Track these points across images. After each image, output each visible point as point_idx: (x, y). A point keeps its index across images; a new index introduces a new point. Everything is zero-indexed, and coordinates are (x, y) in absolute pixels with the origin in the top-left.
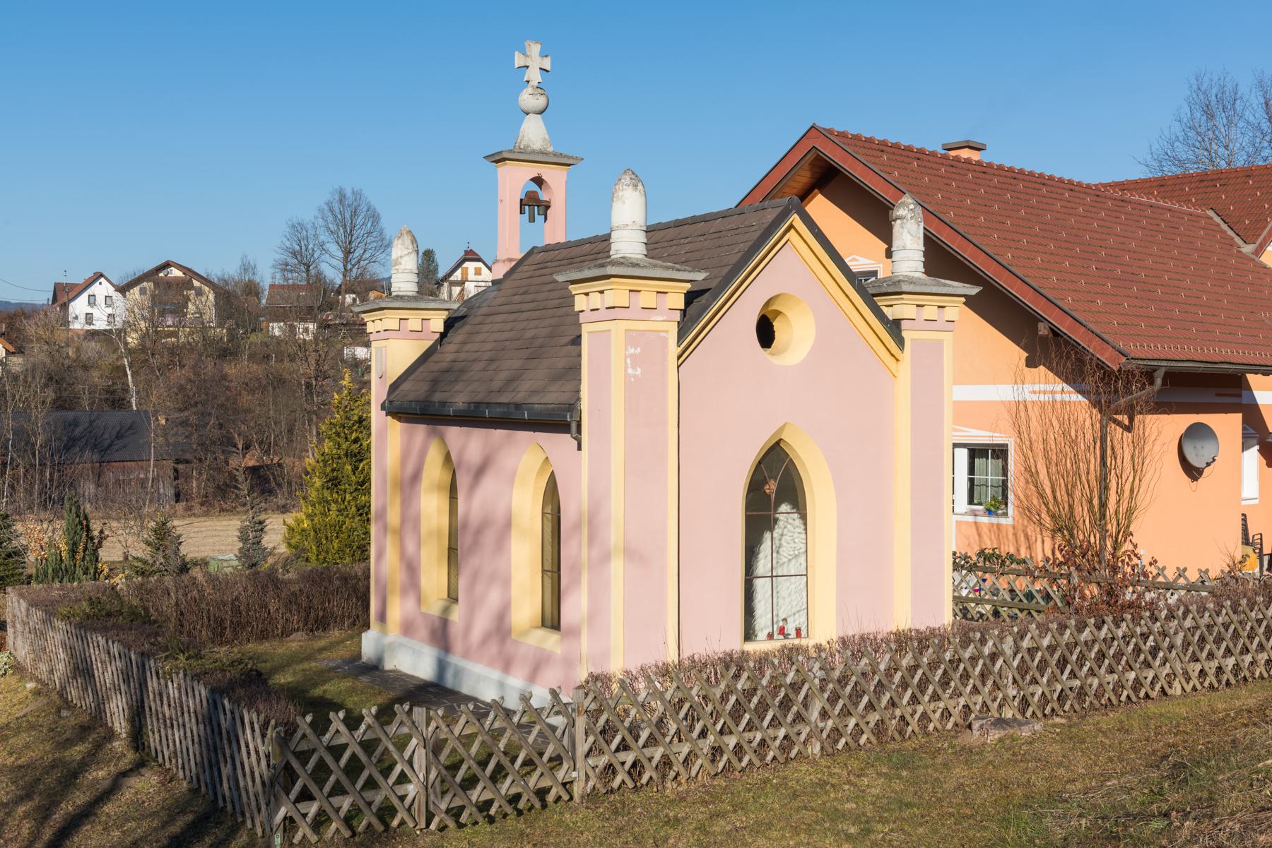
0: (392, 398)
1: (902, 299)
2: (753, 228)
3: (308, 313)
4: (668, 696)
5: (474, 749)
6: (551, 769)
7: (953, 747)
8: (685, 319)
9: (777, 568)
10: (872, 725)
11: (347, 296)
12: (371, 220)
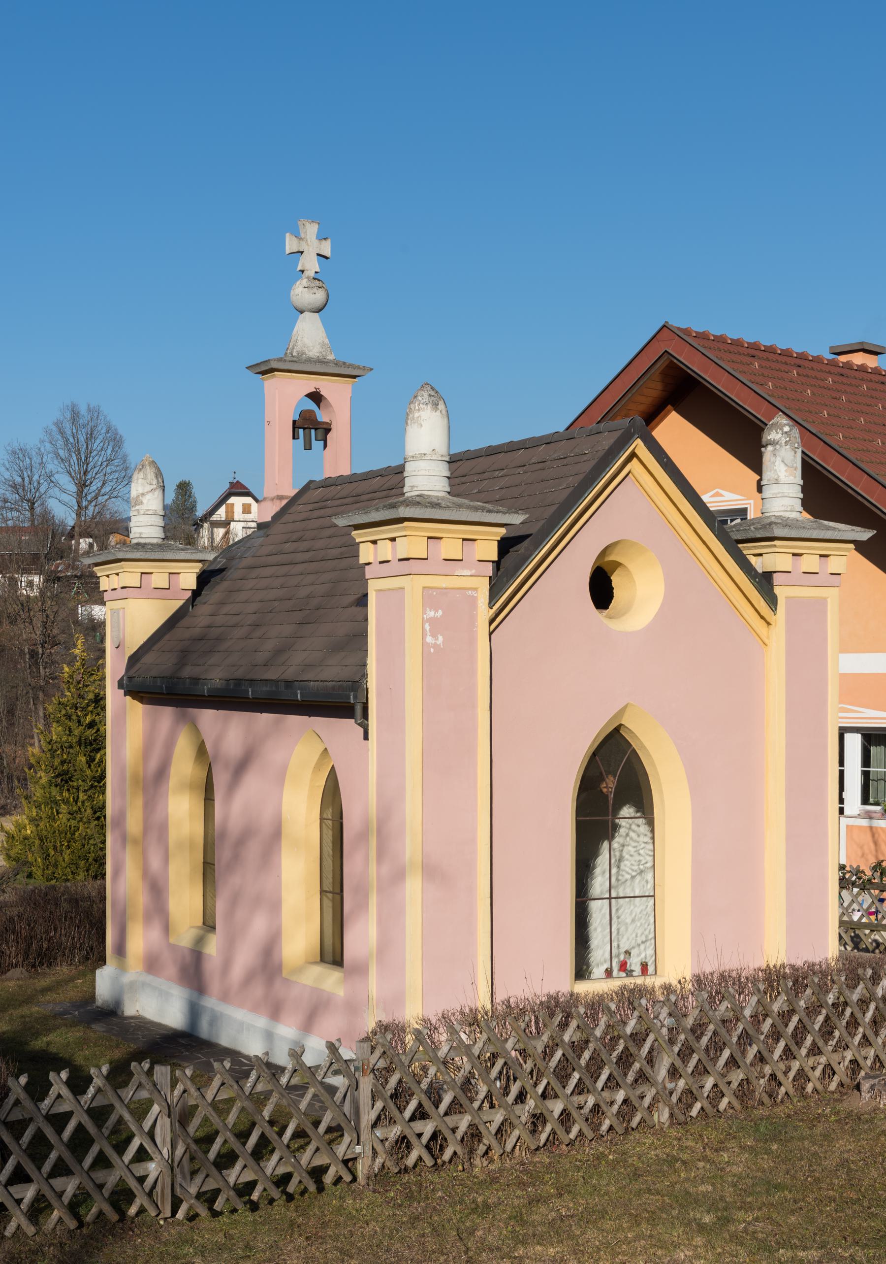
0: (131, 673)
1: (775, 546)
2: (585, 458)
3: (32, 563)
4: (476, 1051)
5: (231, 1118)
6: (330, 1143)
7: (837, 1113)
8: (499, 573)
9: (617, 887)
10: (735, 1085)
11: (81, 540)
12: (111, 444)
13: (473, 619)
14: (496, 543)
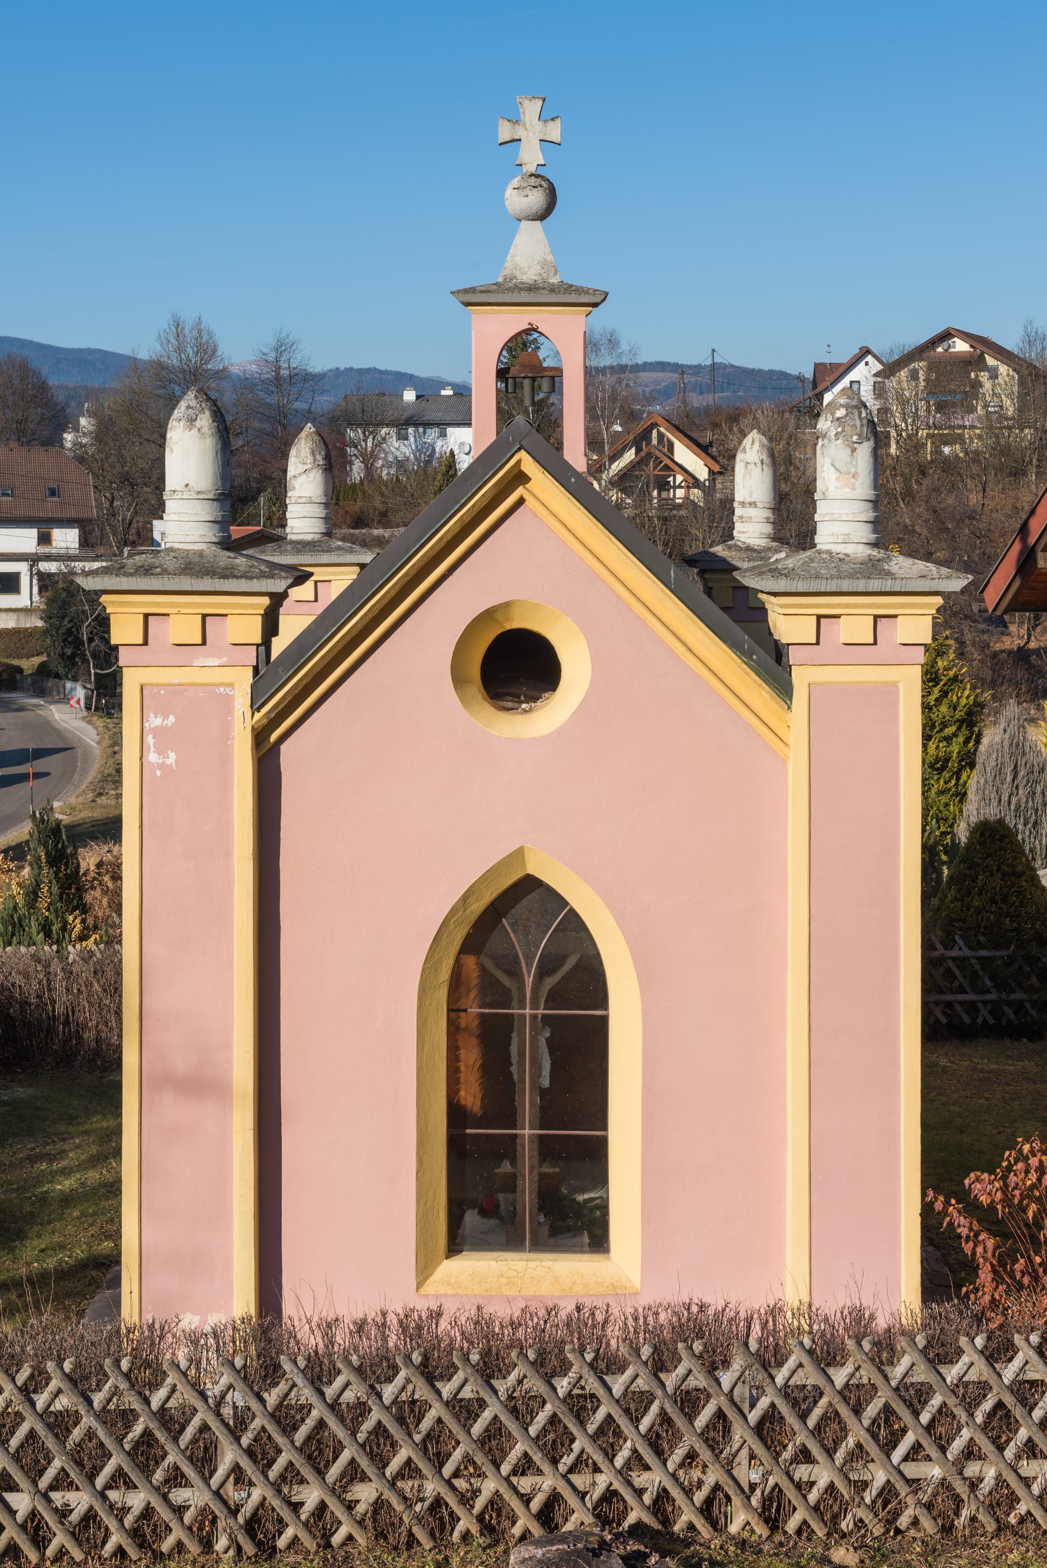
13: (226, 732)
14: (260, 618)
